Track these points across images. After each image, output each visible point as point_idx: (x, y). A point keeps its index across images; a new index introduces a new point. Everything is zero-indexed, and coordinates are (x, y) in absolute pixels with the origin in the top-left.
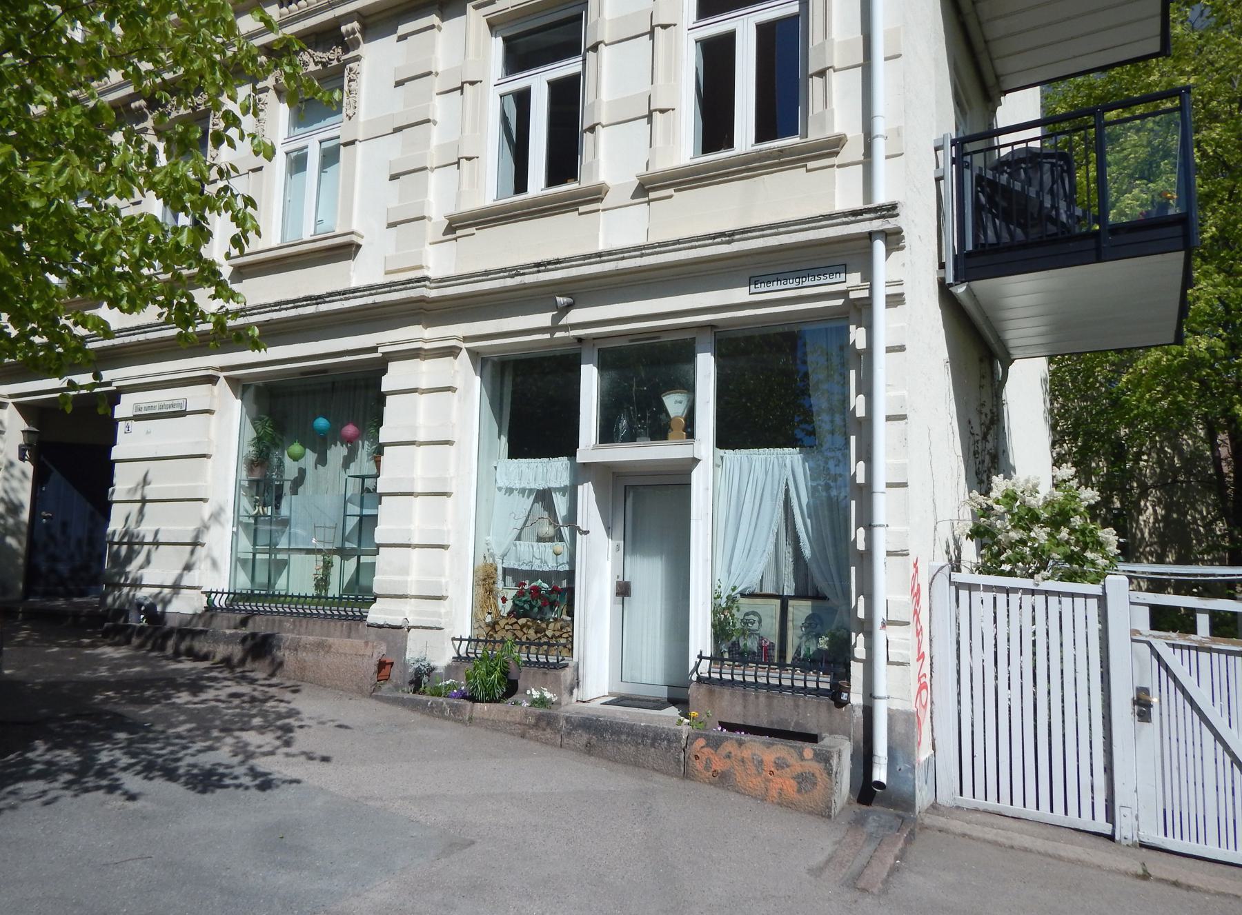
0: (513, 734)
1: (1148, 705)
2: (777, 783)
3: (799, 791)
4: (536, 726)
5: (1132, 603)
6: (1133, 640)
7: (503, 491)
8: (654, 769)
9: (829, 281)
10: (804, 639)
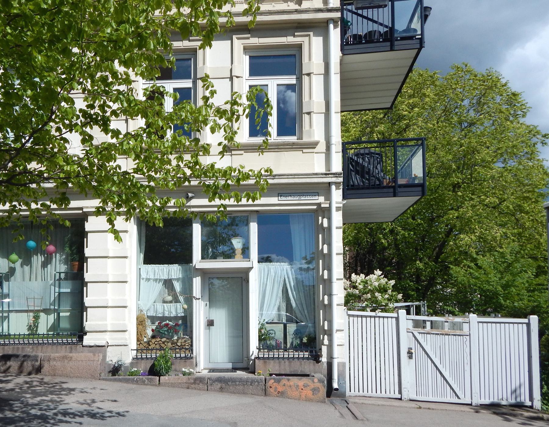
0: (183, 388)
1: (412, 353)
2: (304, 393)
3: (313, 394)
4: (194, 383)
5: (407, 319)
6: (407, 332)
7: (145, 280)
8: (252, 394)
9: (311, 198)
10: (294, 339)
